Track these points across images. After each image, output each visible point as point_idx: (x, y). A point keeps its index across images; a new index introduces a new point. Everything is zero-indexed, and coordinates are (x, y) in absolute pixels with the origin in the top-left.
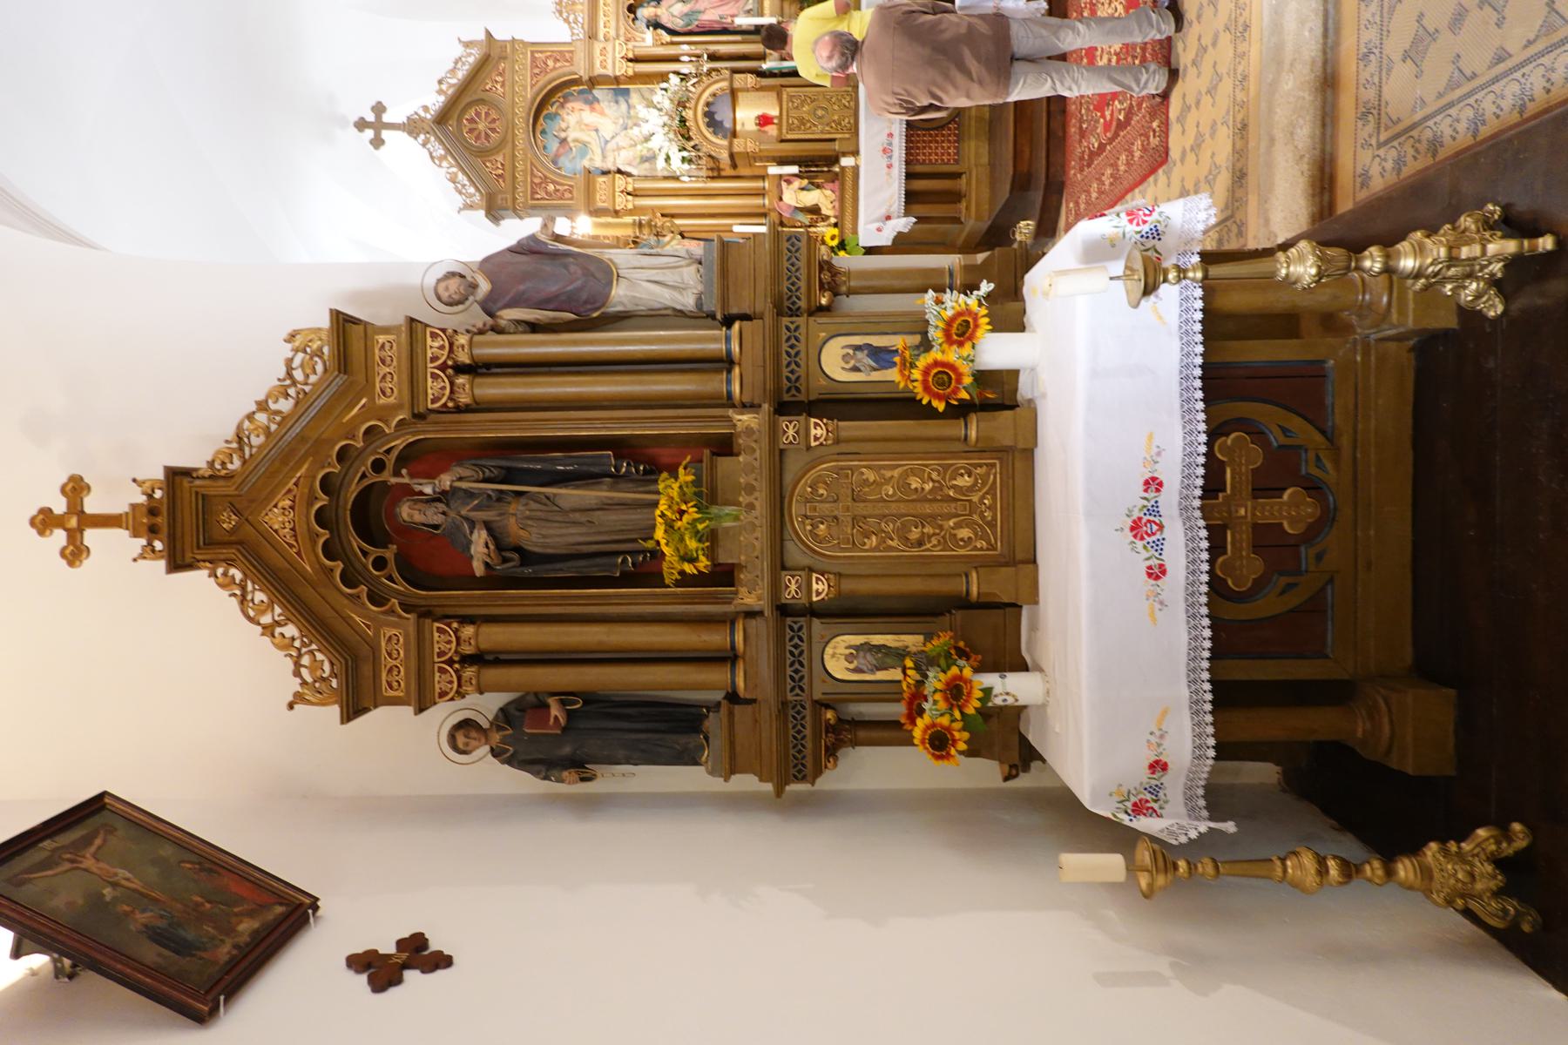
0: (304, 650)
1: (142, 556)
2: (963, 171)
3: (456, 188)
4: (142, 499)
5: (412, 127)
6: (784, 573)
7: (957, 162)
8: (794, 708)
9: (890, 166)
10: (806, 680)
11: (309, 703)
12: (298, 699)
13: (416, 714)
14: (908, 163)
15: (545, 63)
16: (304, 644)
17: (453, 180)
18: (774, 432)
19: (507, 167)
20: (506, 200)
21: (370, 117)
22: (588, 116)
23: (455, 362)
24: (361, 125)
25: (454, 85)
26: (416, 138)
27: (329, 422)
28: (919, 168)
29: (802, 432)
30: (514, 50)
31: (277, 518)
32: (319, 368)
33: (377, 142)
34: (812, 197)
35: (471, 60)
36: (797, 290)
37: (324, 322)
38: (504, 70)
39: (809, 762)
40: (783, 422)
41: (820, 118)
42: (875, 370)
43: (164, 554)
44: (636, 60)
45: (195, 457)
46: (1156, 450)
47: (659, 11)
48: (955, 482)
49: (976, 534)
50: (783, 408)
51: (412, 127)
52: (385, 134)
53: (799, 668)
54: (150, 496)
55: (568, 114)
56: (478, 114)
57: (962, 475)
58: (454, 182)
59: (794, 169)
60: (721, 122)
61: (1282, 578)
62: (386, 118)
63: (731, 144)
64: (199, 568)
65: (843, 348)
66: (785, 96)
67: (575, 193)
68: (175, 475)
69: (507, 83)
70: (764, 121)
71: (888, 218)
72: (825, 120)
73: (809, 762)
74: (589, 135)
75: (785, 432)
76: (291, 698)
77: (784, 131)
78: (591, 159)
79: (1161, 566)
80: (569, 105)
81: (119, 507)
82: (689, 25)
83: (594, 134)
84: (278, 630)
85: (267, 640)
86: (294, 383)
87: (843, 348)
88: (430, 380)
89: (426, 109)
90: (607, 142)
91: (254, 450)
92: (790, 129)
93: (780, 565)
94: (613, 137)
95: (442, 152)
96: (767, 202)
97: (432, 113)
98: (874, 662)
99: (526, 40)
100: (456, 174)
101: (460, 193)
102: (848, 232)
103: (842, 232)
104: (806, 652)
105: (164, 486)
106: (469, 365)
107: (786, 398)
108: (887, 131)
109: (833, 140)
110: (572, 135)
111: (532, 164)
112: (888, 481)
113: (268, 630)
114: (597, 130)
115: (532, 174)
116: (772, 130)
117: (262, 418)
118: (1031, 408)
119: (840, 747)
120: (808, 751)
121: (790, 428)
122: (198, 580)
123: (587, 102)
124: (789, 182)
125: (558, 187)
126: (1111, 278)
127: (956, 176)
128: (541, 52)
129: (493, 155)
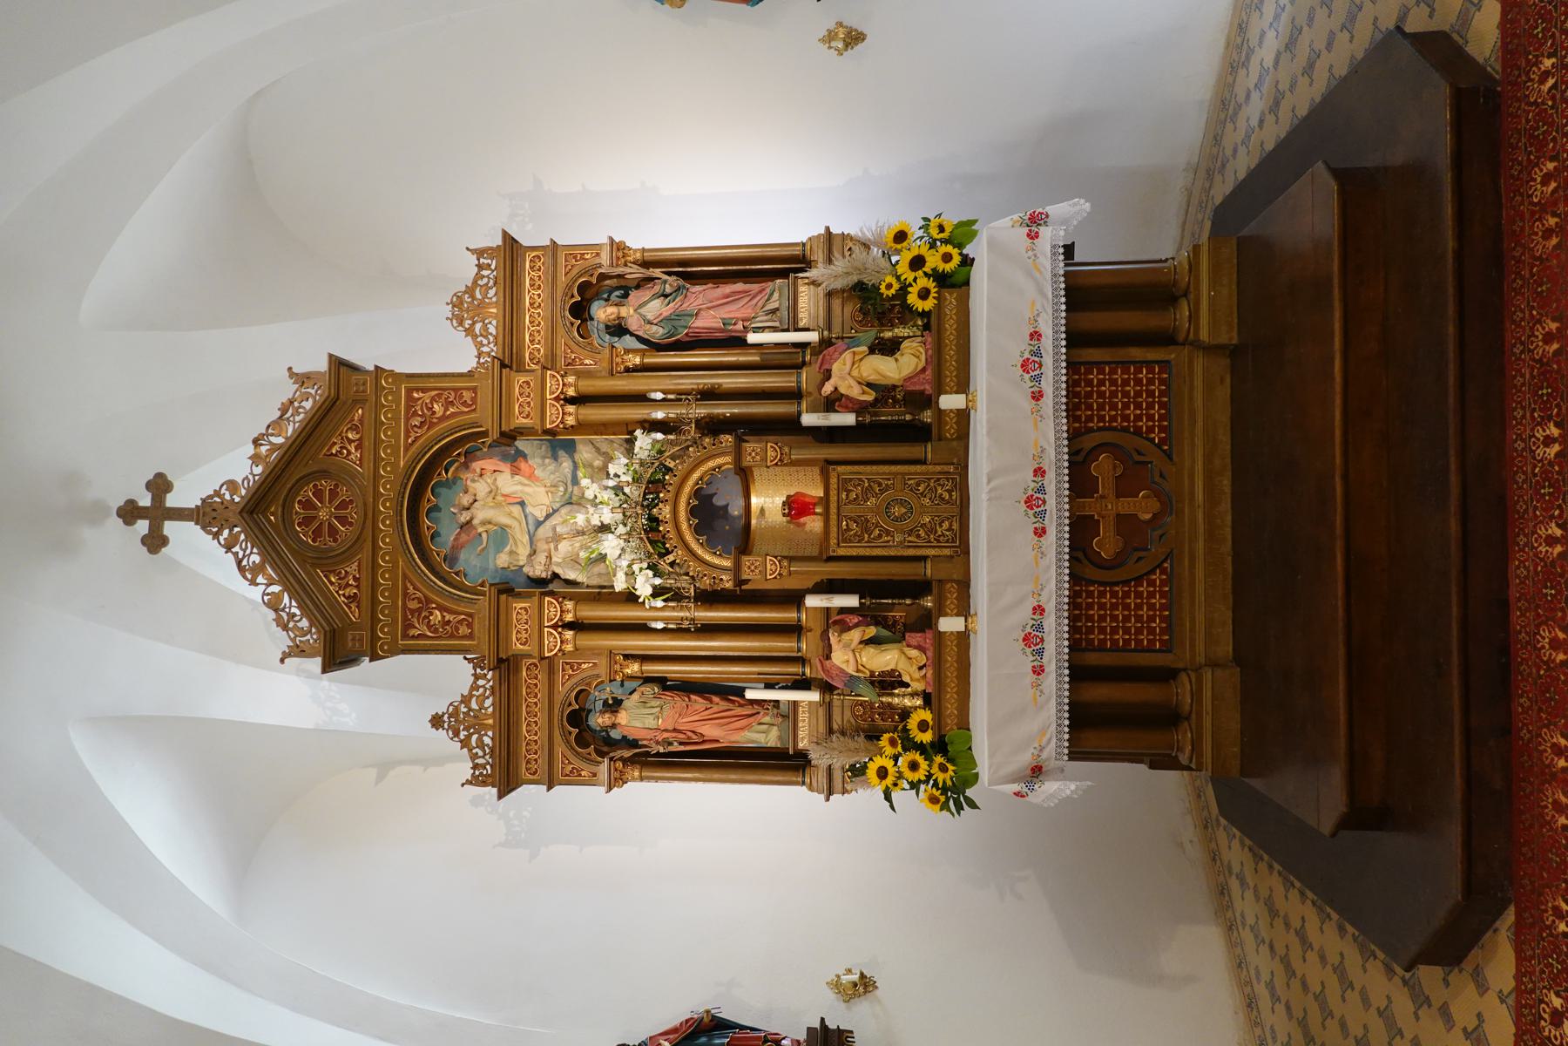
2: (1181, 665)
3: (279, 621)
5: (207, 515)
7: (1167, 648)
9: (1037, 396)
14: (1074, 647)
15: (430, 409)
17: (274, 604)
20: (361, 640)
21: (145, 501)
22: (507, 482)
24: (130, 513)
25: (281, 446)
26: (216, 536)
28: (1093, 659)
30: (378, 387)
33: (156, 542)
34: (885, 659)
35: (308, 405)
38: (361, 420)
41: (897, 519)
44: (580, 400)
46: (1037, 312)
47: (624, 311)
51: (207, 515)
52: (170, 528)
55: (473, 481)
56: (307, 505)
58: (276, 610)
59: (852, 601)
62: (172, 501)
66: (834, 481)
67: (476, 627)
70: (796, 507)
71: (1037, 771)
72: (907, 524)
74: (510, 515)
77: (833, 541)
79: (1040, 392)
80: (477, 466)
83: (516, 510)
89: (232, 485)
90: (539, 524)
92: (844, 538)
94: (548, 517)
95: (256, 558)
96: (808, 671)
97: (243, 492)
99: (398, 370)
101: (285, 628)
102: (950, 723)
108: (1033, 603)
109: (924, 558)
110: (480, 514)
111: (405, 576)
114: (522, 504)
115: (405, 594)
116: (814, 524)
123: (505, 458)
124: (846, 628)
127: (1167, 675)
128: (424, 390)
129: (342, 562)
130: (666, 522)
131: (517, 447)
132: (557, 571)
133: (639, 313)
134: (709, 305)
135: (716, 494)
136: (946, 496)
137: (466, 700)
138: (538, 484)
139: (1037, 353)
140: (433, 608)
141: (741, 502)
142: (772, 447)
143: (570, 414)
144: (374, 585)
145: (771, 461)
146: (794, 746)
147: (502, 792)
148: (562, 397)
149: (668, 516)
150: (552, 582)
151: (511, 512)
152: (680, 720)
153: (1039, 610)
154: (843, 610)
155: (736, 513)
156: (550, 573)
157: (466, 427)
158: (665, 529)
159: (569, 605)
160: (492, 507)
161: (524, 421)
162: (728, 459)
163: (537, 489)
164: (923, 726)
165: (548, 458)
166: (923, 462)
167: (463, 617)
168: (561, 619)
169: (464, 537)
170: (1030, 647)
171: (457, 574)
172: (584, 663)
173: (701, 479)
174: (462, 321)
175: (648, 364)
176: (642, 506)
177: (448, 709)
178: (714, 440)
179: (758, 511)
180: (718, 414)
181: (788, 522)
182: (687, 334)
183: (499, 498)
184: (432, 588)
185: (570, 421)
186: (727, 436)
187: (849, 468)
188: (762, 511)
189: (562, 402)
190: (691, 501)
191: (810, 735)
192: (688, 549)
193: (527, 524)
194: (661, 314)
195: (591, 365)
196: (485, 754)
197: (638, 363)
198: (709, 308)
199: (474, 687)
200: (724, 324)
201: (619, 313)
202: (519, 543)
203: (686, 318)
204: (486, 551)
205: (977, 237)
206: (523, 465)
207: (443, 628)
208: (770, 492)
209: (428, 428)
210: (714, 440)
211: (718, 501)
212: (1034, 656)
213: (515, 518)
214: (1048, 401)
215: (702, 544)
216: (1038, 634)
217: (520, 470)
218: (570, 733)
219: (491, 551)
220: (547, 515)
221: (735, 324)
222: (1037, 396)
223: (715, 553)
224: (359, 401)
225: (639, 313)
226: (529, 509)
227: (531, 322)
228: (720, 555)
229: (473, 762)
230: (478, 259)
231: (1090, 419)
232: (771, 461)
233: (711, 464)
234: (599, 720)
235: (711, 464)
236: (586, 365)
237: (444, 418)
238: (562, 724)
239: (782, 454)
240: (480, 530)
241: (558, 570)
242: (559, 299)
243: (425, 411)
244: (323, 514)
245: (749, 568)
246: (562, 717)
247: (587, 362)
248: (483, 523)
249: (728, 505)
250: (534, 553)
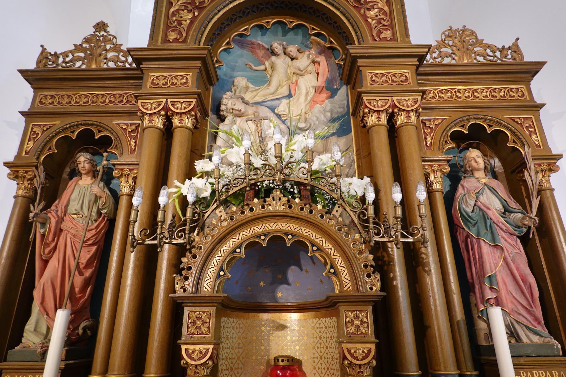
12: (44, 49)
15: (373, 7)
27: (533, 322)
60: (285, 281)
74: (280, 86)
76: (45, 47)
78: (247, 88)
80: (322, 59)
82: (466, 220)
83: (284, 91)
90: (272, 109)
94: (279, 116)
110: (281, 62)
114: (290, 96)
130: (263, 207)
131: (339, 89)
132: (227, 119)
133: (483, 189)
134: (509, 260)
135: (301, 270)
138: (308, 107)
140: (194, 13)
141: (291, 301)
142: (370, 351)
143: (379, 119)
145: (349, 351)
146: (6, 369)
147: (25, 74)
148: (396, 110)
149: (270, 207)
150: (218, 118)
151: (282, 87)
152: (69, 236)
155: (279, 294)
156: (225, 113)
157: (359, 33)
158: (256, 205)
159: (188, 122)
160: (287, 72)
161: (369, 79)
162: (348, 285)
163: (303, 106)
165: (332, 114)
167: (184, 35)
168: (173, 113)
169: (261, 53)
171: (228, 43)
172: (135, 142)
173: (318, 249)
174: (451, 37)
175: (435, 197)
176: (284, 181)
177: (110, 35)
178: (372, 266)
179: (281, 322)
180: (394, 272)
181: (268, 362)
182: (468, 236)
183: (294, 78)
185: (371, 120)
186: (379, 284)
188: (283, 327)
189: (391, 110)
190: (290, 237)
192: (228, 234)
193: (272, 100)
194: (489, 209)
195: (426, 142)
196: (66, 63)
197: (434, 187)
198: (505, 260)
200: (489, 276)
201: (478, 170)
202: (255, 93)
203: (489, 235)
204: (249, 70)
206: (324, 95)
207: (176, 20)
208: (305, 338)
209: (356, 6)
210: (372, 266)
211: (292, 273)
213: (277, 90)
215: (235, 251)
217: (320, 93)
218: (73, 132)
219: (250, 74)
220: (280, 115)
221: (491, 288)
223: (221, 269)
225: (483, 189)
226: (285, 101)
227: (459, 91)
228: (219, 276)
229: (61, 54)
230: (509, 48)
232: (349, 351)
233: (340, 262)
235: (340, 262)
236: (426, 138)
237: (365, 17)
238: (81, 124)
239: (360, 366)
240: (267, 63)
242: (490, 114)
243: (371, 4)
245: (199, 318)
246: (88, 124)
247: (429, 139)
248: (273, 67)
249: (289, 284)
250: (247, 103)
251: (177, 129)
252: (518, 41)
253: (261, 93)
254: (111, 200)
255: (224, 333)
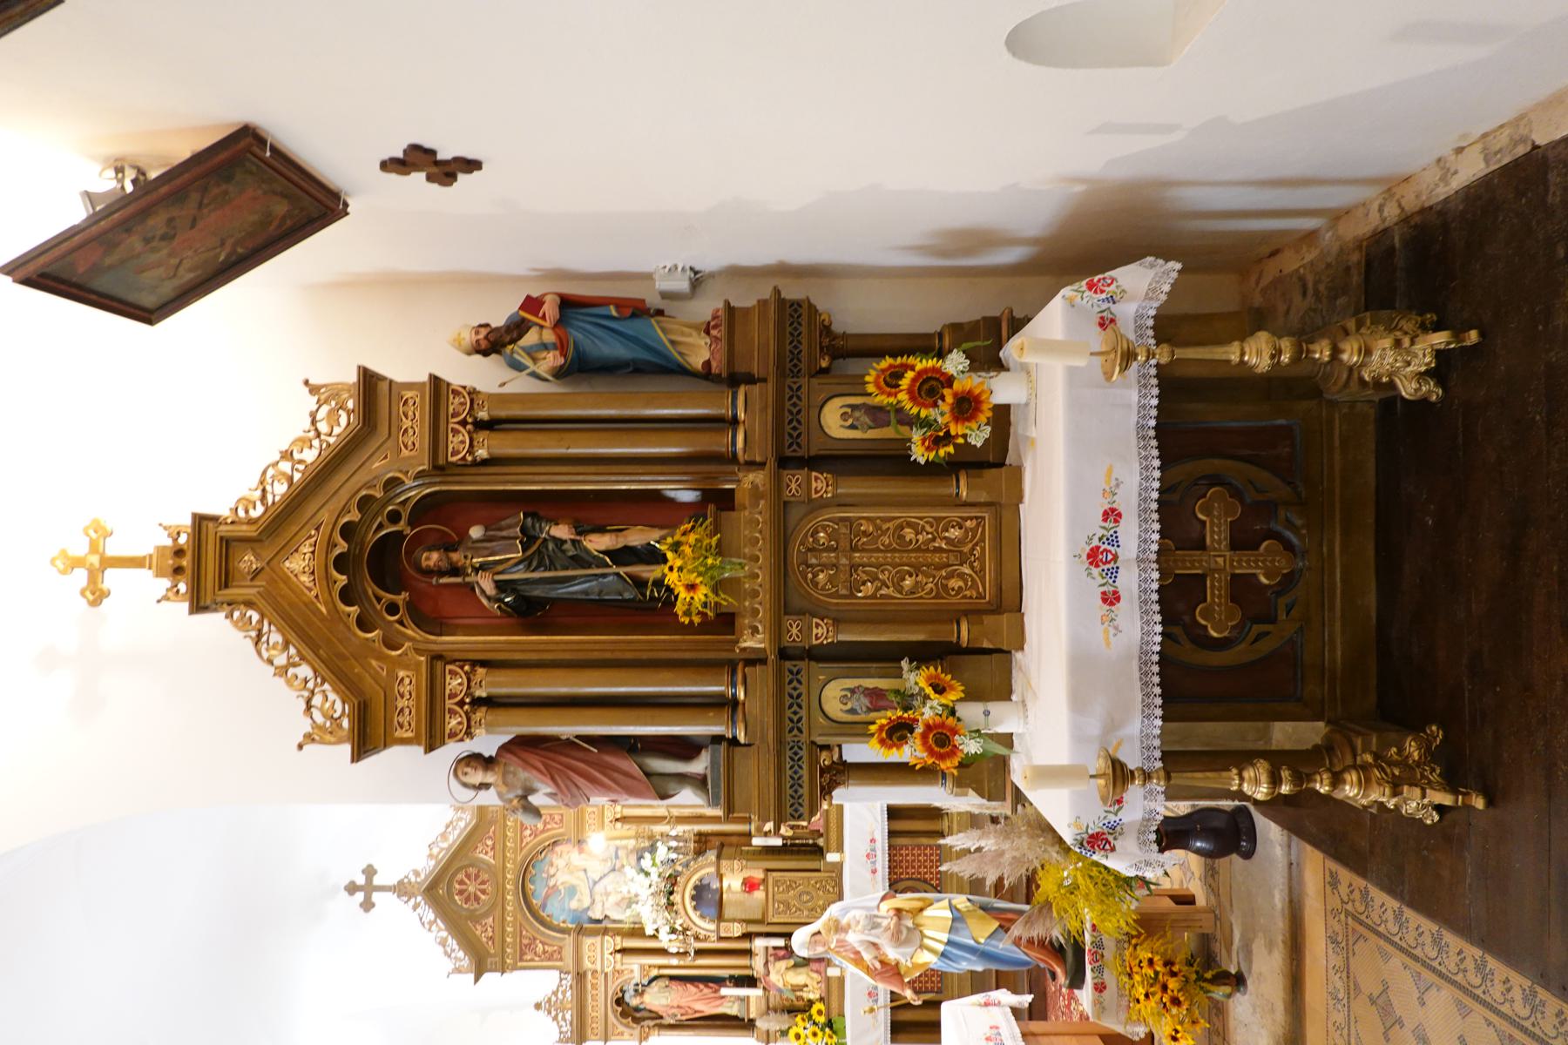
0: (316, 690)
1: (166, 598)
4: (169, 542)
5: (401, 889)
6: (787, 617)
8: (791, 748)
9: (874, 872)
10: (803, 697)
11: (322, 742)
12: (309, 738)
13: (426, 752)
16: (316, 685)
17: (443, 943)
18: (778, 485)
19: (496, 929)
22: (575, 857)
23: (476, 418)
24: (352, 888)
29: (804, 486)
31: (299, 564)
32: (343, 420)
33: (367, 905)
35: (462, 824)
36: (798, 317)
37: (352, 377)
39: (805, 801)
40: (787, 475)
42: (870, 428)
43: (188, 596)
45: (219, 506)
48: (947, 534)
49: (966, 585)
50: (784, 462)
51: (401, 889)
52: (376, 897)
53: (798, 710)
54: (175, 540)
57: (953, 527)
58: (444, 946)
61: (1255, 627)
62: (377, 881)
63: (718, 927)
64: (215, 610)
65: (841, 407)
68: (200, 520)
69: (497, 847)
70: (750, 886)
73: (805, 801)
75: (788, 486)
76: (300, 739)
77: (770, 913)
81: (145, 548)
83: (582, 874)
84: (291, 671)
85: (281, 681)
86: (318, 435)
87: (841, 407)
88: (451, 397)
89: (417, 874)
90: (595, 883)
91: (277, 498)
93: (785, 606)
94: (601, 878)
98: (869, 705)
100: (446, 939)
101: (449, 956)
103: (828, 1009)
104: (804, 719)
105: (189, 530)
106: (488, 422)
107: (788, 453)
111: (521, 925)
112: (884, 533)
113: (282, 671)
116: (759, 895)
117: (286, 466)
118: (1018, 472)
119: (834, 788)
120: (805, 791)
121: (794, 481)
122: (215, 621)
125: (546, 948)
126: (1092, 354)
136: (831, 890)
137: (555, 993)
139: (874, 850)
144: (503, 930)
153: (1112, 515)
154: (775, 948)
159: (618, 939)
164: (820, 1013)
166: (819, 870)
170: (1097, 566)
184: (538, 931)
187: (779, 874)
191: (757, 1010)
199: (560, 985)
205: (952, 321)
212: (1103, 578)
214: (879, 873)
216: (1109, 548)
219: (567, 900)
222: (874, 872)
224: (491, 823)
226: (589, 874)
231: (902, 874)
234: (634, 1002)
241: (608, 913)
244: (471, 889)
248: (562, 883)
251: (736, 935)
252: (310, 382)
253: (584, 889)
254: (660, 980)
255: (731, 916)
